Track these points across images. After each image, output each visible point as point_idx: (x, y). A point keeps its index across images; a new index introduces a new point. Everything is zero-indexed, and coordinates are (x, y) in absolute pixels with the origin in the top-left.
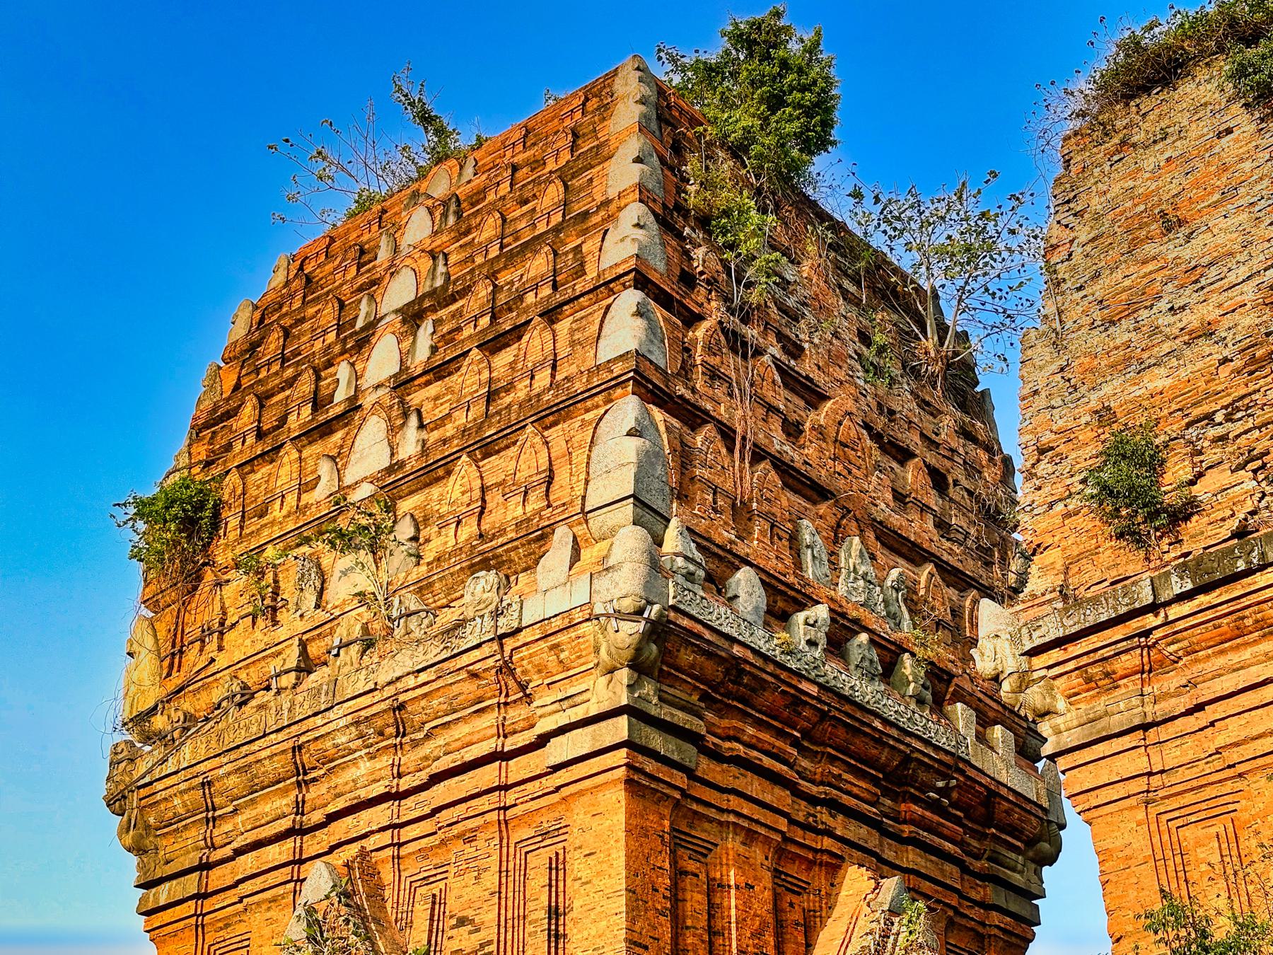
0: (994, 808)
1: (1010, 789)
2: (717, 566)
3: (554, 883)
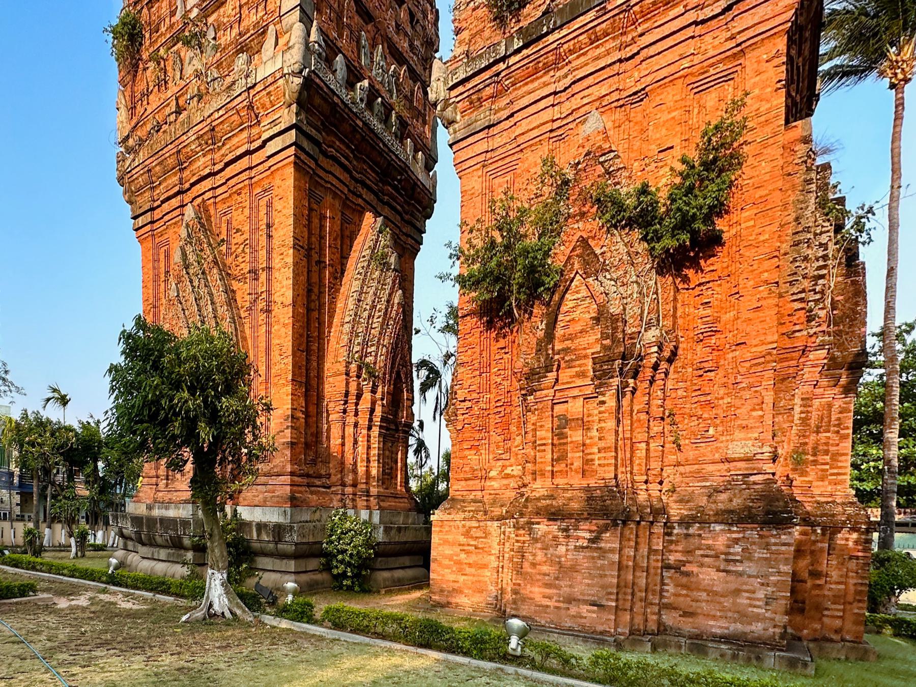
2: (330, 50)
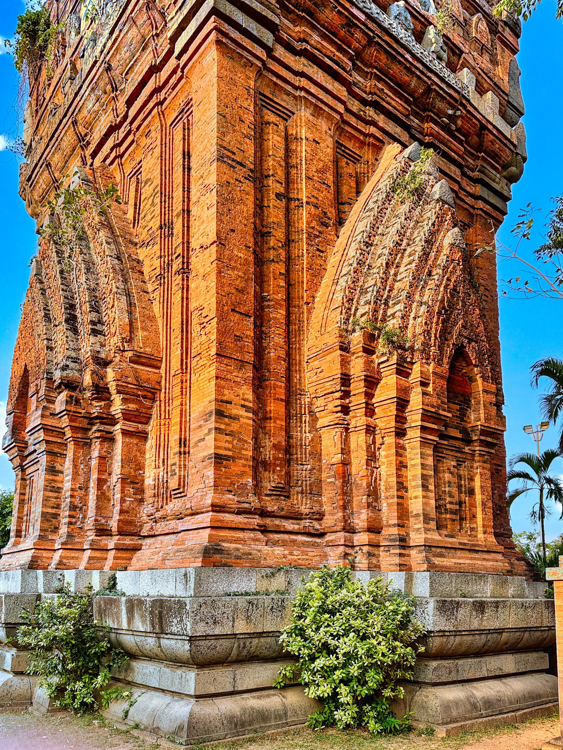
0: (484, 138)
1: (494, 127)
3: (186, 137)
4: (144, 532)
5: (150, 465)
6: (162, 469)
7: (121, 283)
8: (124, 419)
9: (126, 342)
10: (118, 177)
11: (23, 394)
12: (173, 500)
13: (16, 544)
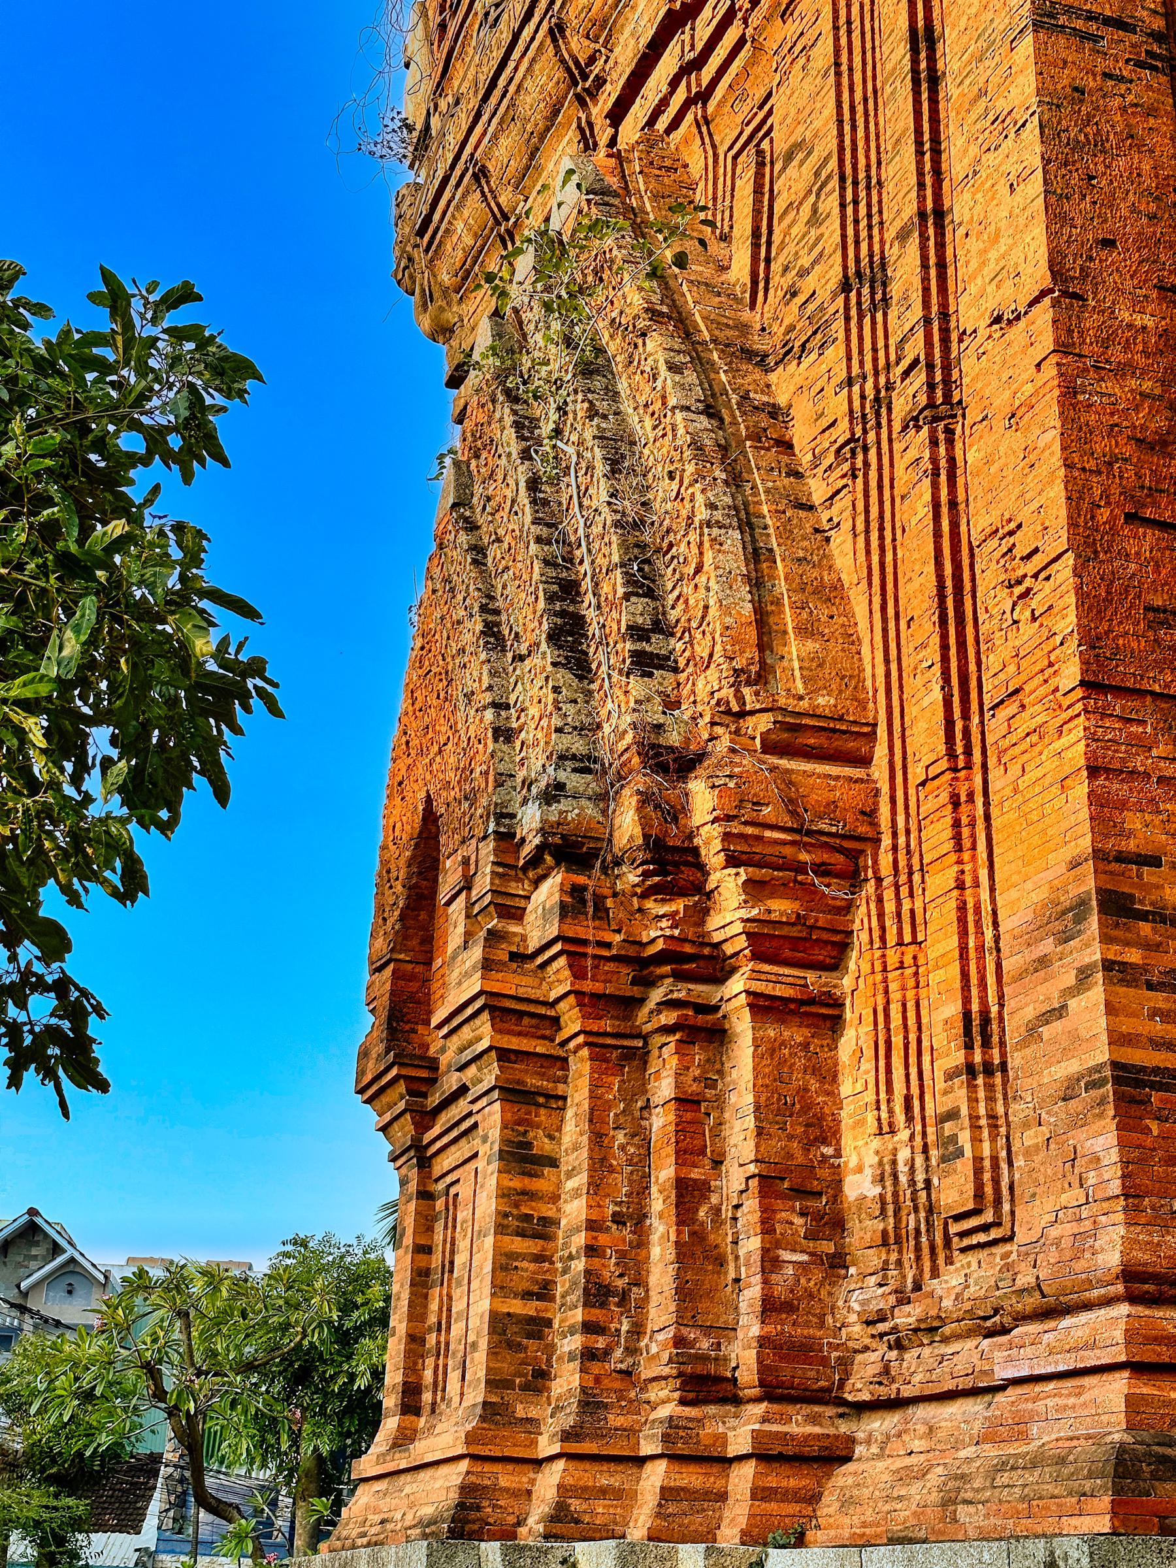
4: (859, 1389)
5: (861, 1123)
6: (904, 1135)
7: (720, 487)
8: (755, 956)
9: (748, 683)
10: (696, 160)
11: (420, 897)
12: (960, 1259)
13: (403, 1439)
